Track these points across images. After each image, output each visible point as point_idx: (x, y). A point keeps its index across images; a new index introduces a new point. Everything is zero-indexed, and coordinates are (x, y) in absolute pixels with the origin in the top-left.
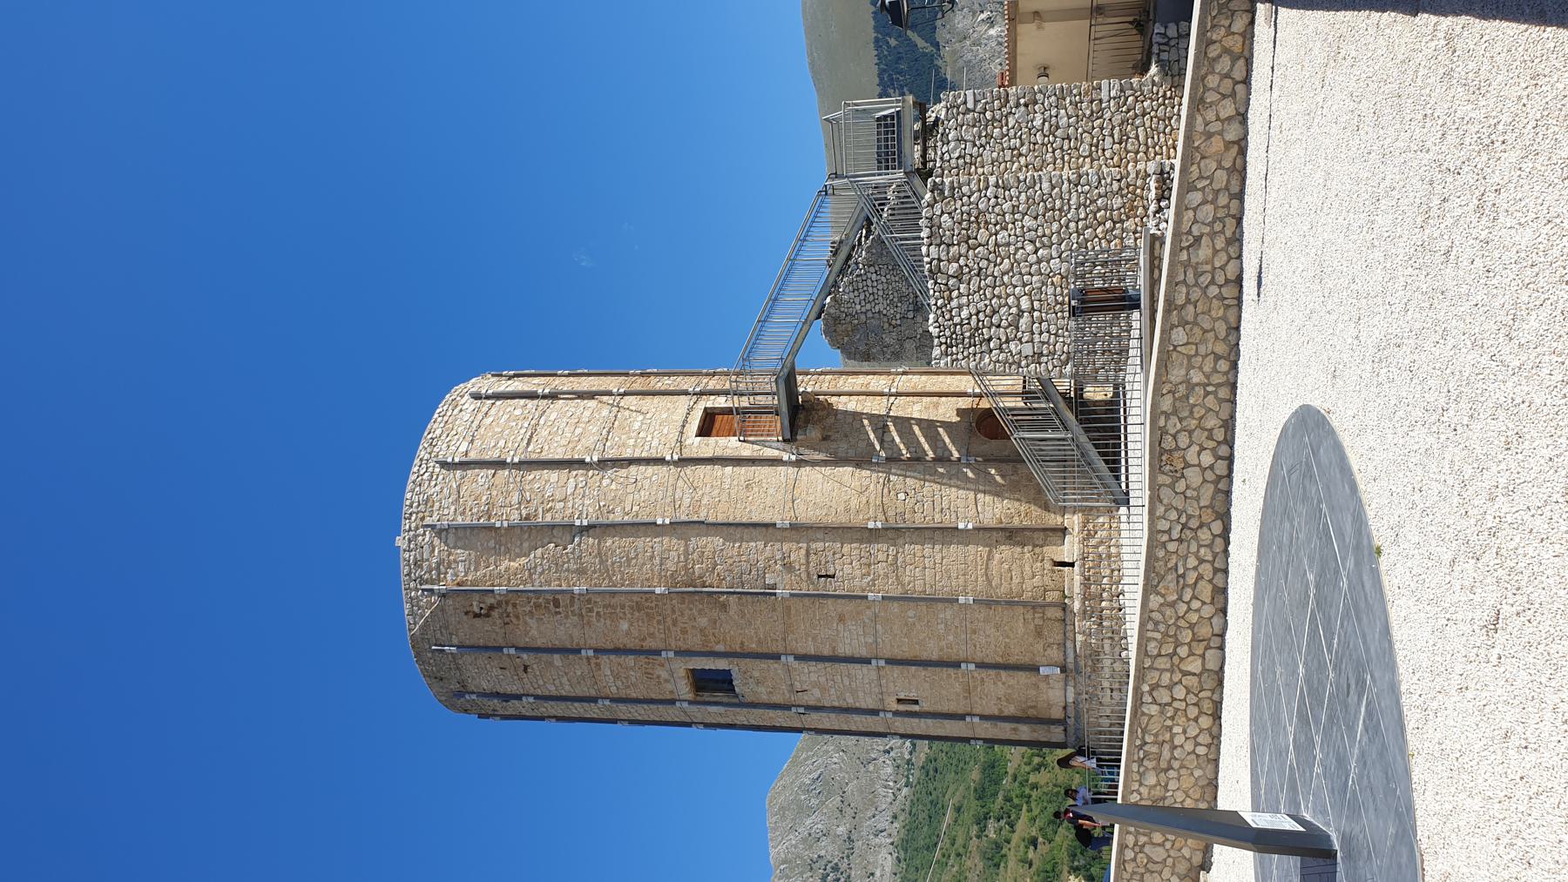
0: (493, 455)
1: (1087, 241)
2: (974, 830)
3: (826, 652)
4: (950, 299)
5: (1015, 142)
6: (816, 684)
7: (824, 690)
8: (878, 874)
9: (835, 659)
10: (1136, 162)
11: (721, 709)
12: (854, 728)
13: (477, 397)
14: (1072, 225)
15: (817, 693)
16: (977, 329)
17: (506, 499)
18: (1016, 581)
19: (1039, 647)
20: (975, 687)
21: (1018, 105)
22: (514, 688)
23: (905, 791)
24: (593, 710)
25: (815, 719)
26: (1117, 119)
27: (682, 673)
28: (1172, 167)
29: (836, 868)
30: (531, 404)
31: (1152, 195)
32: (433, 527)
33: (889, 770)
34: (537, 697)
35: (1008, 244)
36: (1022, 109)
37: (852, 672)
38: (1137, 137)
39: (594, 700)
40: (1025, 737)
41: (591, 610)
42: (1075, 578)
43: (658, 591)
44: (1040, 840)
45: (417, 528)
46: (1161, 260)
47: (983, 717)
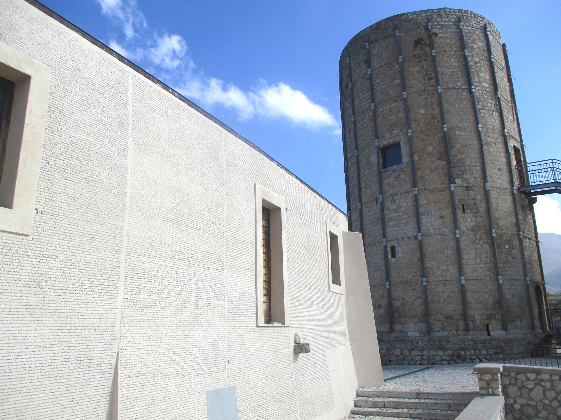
3: (421, 210)
6: (399, 206)
7: (396, 211)
9: (418, 215)
19: (440, 317)
27: (397, 140)
41: (428, 95)
45: (456, 15)
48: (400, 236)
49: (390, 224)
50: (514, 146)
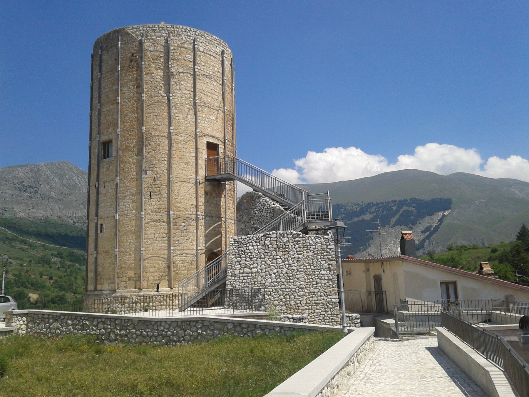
0: (198, 60)
1: (278, 292)
2: (55, 252)
4: (256, 242)
5: (315, 264)
7: (105, 195)
8: (34, 210)
10: (308, 309)
11: (96, 153)
12: (90, 207)
13: (223, 52)
14: (284, 286)
15: (104, 192)
16: (244, 253)
17: (180, 65)
18: (151, 270)
20: (108, 255)
21: (329, 264)
22: (104, 68)
23: (72, 221)
24: (95, 102)
25: (93, 192)
26: (323, 301)
28: (306, 323)
29: (36, 192)
30: (220, 75)
31: (294, 316)
32: (169, 37)
33: (80, 214)
34: (100, 79)
35: (277, 263)
36: (328, 266)
37: (112, 206)
38: (317, 309)
39: (100, 102)
40: (89, 274)
42: (152, 292)
43: (143, 128)
44: (52, 281)
45: (168, 30)
46: (261, 319)
47: (96, 258)
48: (106, 216)
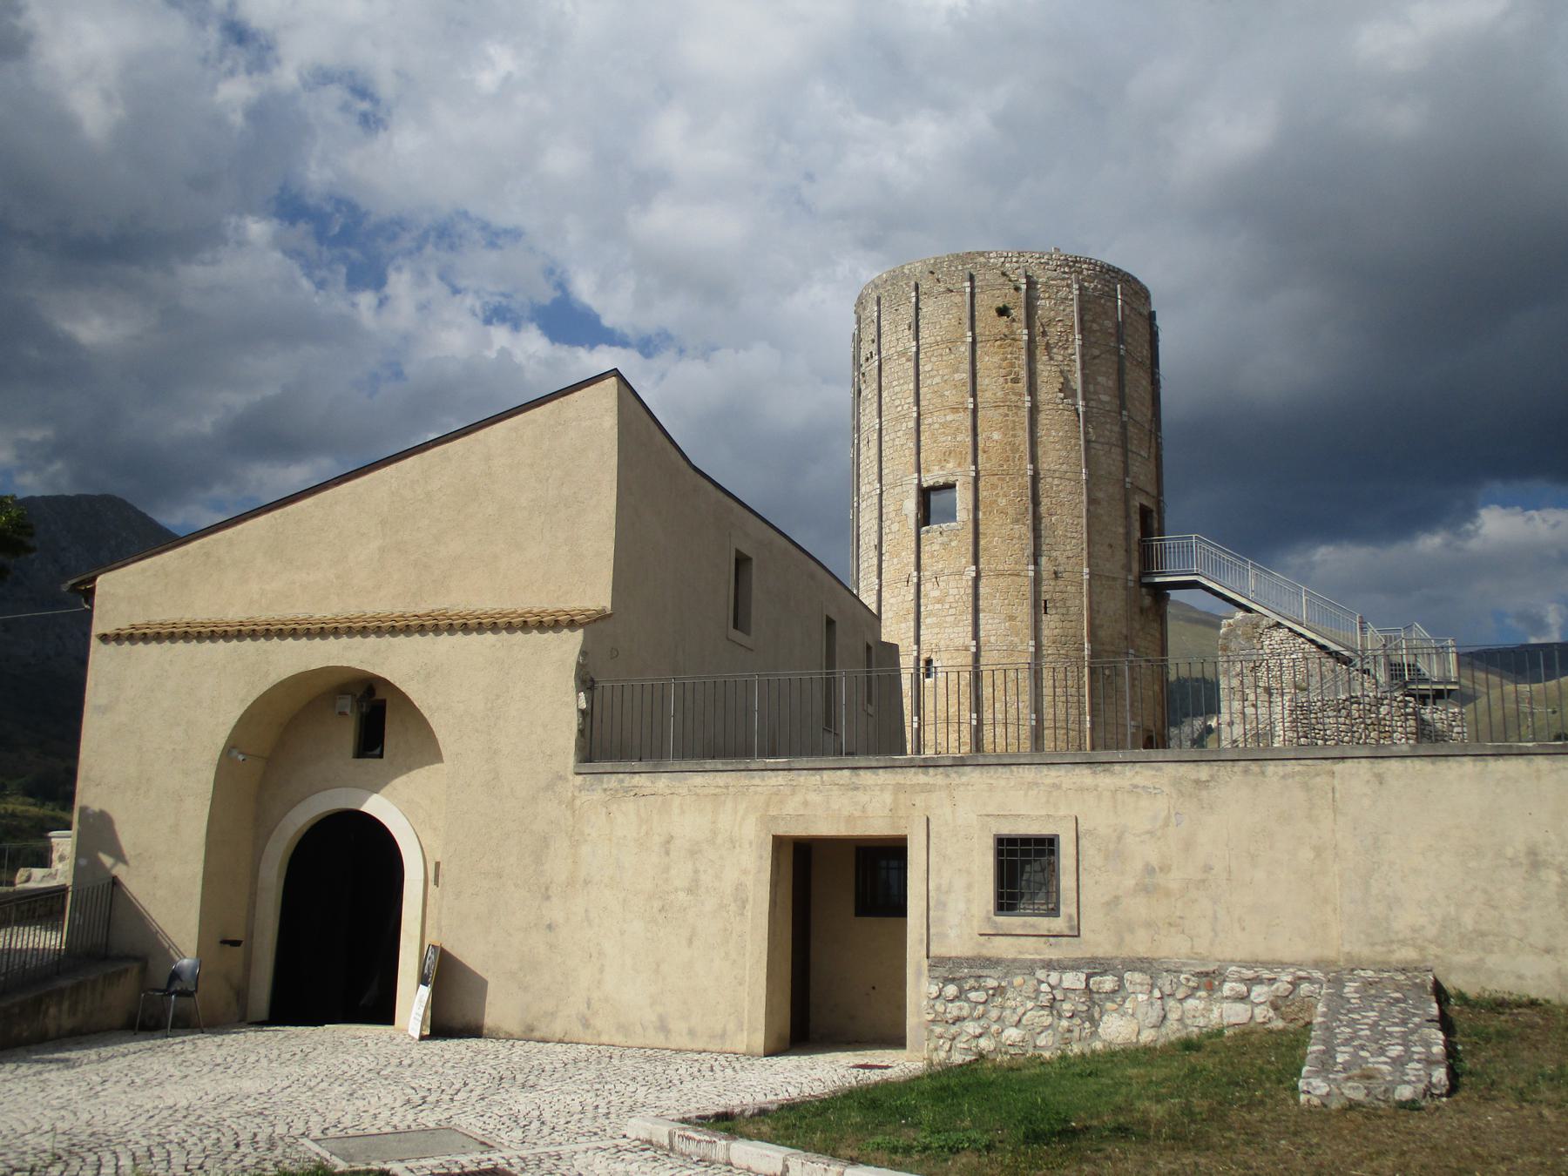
7: (940, 601)
27: (951, 479)
49: (928, 621)
50: (1142, 506)
